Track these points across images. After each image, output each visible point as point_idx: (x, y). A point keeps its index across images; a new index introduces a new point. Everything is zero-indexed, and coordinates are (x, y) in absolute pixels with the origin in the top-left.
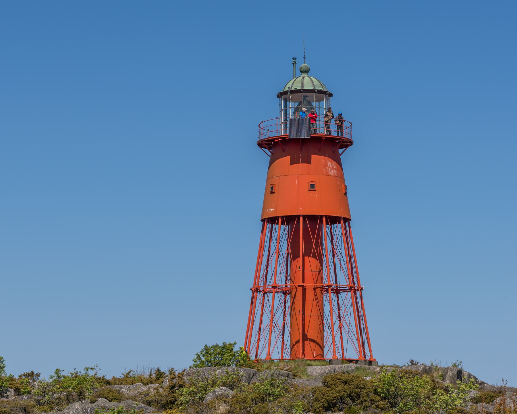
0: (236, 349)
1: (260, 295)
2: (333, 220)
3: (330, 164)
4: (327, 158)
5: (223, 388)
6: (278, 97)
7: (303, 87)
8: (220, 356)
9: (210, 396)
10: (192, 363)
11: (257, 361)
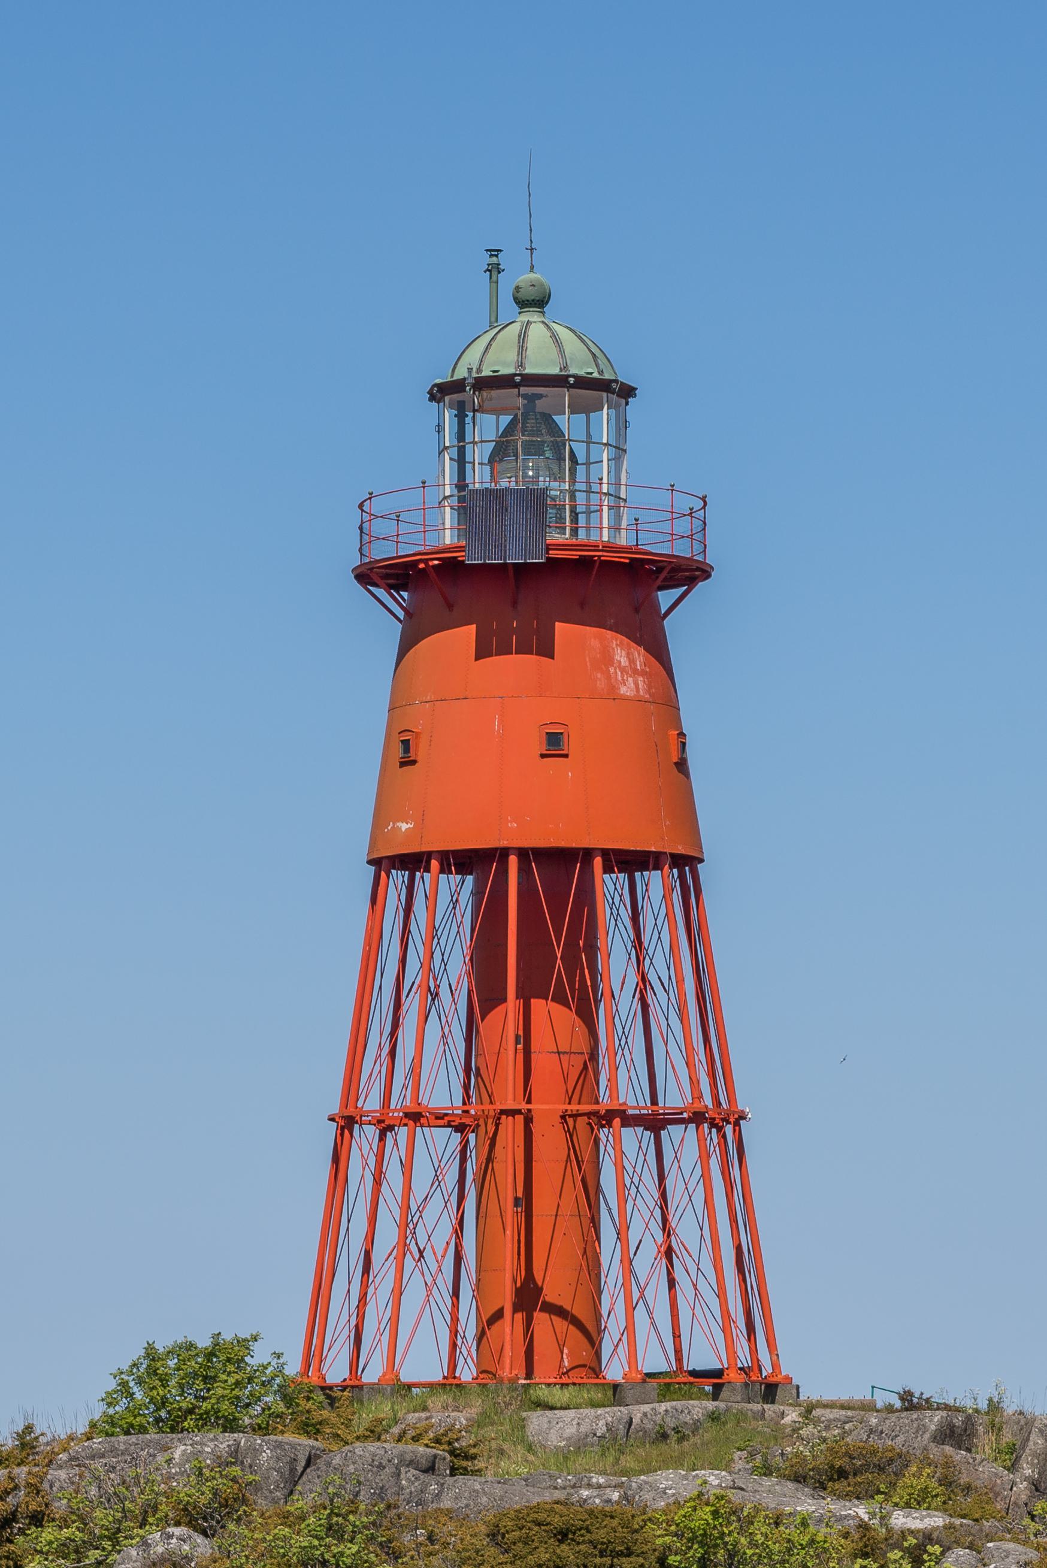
0: (259, 1356)
2: (630, 862)
3: (621, 657)
4: (609, 634)
5: (177, 1531)
6: (432, 398)
7: (521, 365)
8: (199, 1385)
9: (130, 1558)
10: (98, 1411)
11: (354, 1387)
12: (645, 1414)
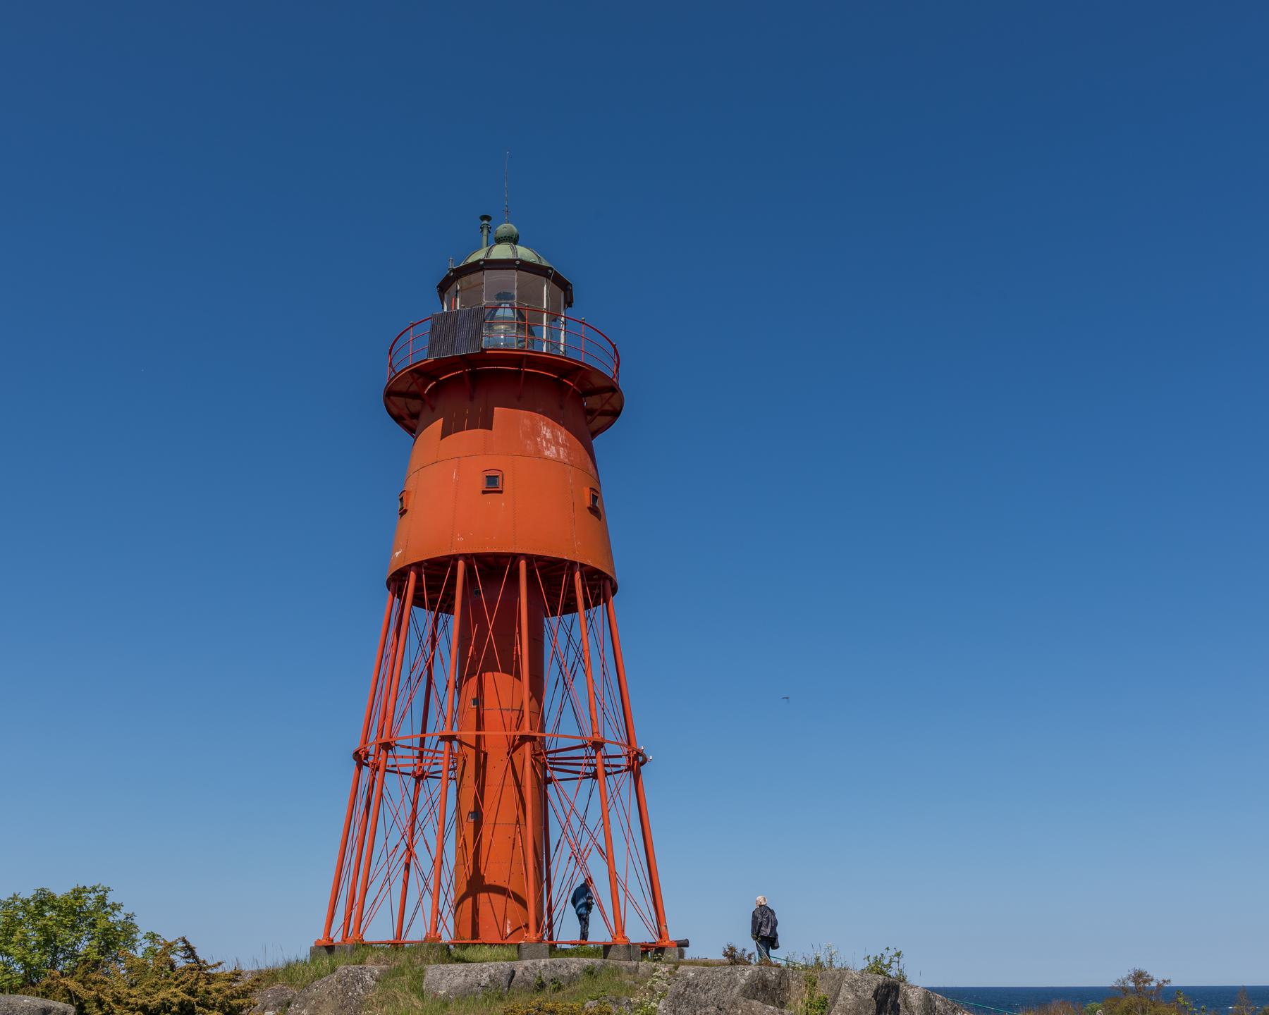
1: (366, 771)
12: (526, 968)
